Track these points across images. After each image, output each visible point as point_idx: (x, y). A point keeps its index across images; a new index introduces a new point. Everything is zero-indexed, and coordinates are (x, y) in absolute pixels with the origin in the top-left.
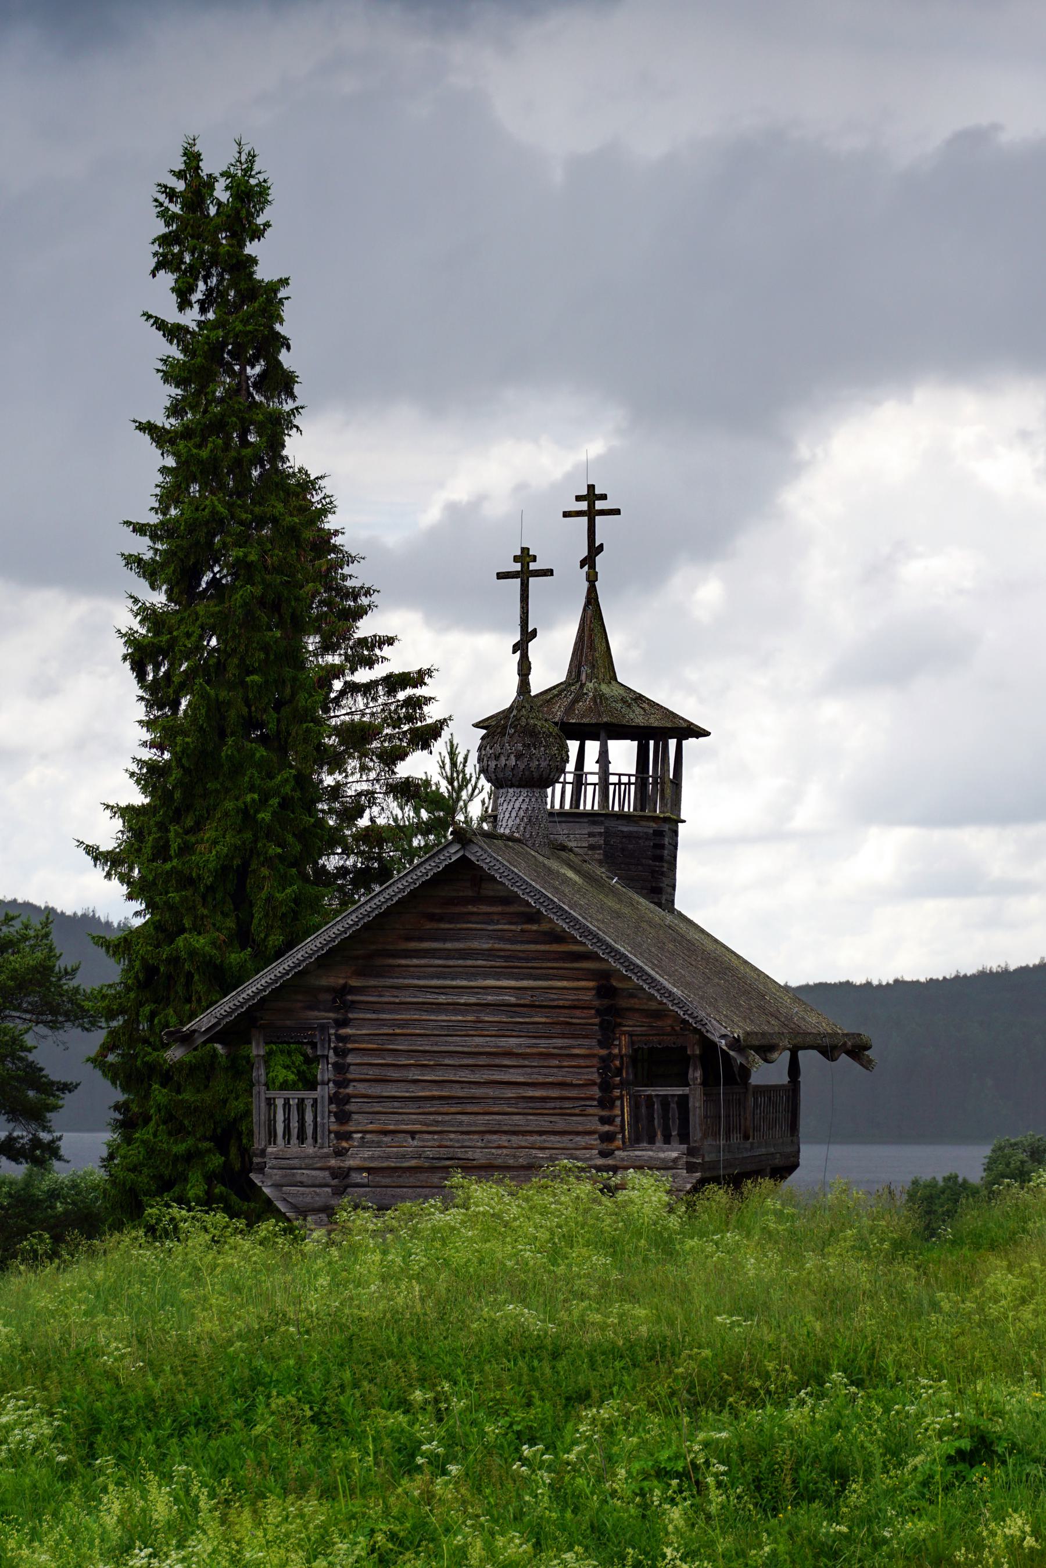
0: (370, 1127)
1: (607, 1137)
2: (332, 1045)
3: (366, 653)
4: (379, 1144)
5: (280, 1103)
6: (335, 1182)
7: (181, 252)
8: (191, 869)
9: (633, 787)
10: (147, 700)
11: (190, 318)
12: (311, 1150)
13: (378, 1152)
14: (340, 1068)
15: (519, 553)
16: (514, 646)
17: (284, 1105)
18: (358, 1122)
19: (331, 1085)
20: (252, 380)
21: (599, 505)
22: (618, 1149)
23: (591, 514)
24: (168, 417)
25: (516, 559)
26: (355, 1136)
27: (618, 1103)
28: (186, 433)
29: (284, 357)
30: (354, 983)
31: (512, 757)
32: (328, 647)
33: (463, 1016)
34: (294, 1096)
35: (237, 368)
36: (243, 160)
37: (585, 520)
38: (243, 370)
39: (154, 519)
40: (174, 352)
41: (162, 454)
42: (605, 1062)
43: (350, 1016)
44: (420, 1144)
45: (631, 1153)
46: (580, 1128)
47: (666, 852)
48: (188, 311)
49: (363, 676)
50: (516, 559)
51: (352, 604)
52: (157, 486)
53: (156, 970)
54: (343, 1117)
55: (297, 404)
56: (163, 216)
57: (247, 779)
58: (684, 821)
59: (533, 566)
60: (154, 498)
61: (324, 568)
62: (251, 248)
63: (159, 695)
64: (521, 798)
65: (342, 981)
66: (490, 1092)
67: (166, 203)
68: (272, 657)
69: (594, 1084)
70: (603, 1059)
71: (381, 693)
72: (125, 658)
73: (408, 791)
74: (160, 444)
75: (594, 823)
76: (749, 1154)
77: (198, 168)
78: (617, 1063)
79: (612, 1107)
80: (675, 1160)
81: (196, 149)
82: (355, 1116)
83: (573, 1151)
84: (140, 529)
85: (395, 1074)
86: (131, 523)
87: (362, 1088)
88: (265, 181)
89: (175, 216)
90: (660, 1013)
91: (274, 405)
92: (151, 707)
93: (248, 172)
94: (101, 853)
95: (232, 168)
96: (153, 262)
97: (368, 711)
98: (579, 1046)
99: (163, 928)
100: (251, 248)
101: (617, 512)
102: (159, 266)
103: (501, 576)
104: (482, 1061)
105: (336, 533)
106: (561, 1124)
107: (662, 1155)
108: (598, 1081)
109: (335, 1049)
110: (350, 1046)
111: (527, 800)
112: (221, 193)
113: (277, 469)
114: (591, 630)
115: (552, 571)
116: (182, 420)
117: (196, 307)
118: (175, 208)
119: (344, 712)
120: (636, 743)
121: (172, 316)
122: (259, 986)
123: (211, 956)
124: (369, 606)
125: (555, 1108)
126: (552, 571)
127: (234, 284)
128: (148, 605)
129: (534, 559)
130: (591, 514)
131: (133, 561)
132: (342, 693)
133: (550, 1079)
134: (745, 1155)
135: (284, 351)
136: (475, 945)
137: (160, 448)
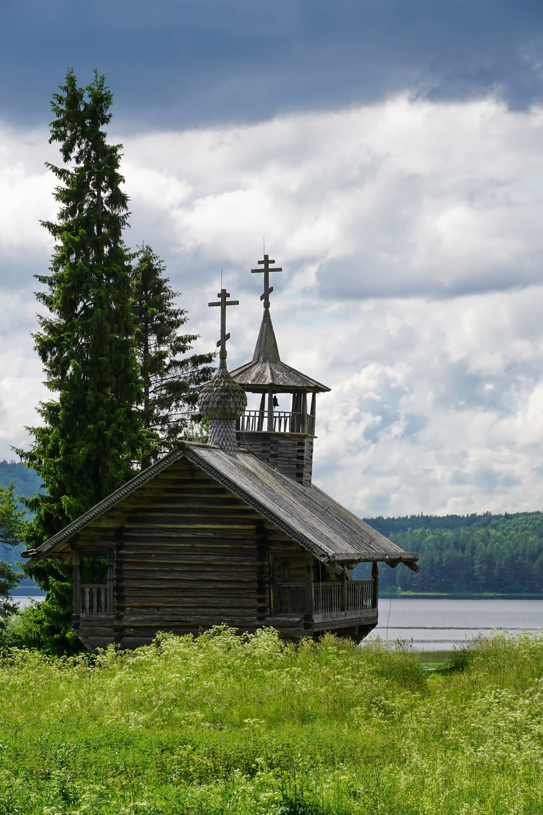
0: (135, 604)
1: (262, 610)
2: (115, 560)
3: (182, 344)
4: (140, 613)
5: (87, 590)
6: (115, 634)
7: (66, 131)
8: (70, 462)
9: (257, 418)
10: (49, 371)
11: (71, 166)
12: (103, 616)
13: (139, 618)
14: (119, 571)
15: (220, 292)
16: (218, 343)
17: (89, 592)
18: (128, 602)
19: (114, 581)
20: (105, 199)
21: (271, 266)
22: (268, 616)
24: (59, 219)
25: (219, 295)
26: (127, 609)
27: (268, 591)
28: (68, 228)
30: (127, 526)
31: (215, 403)
32: (160, 342)
33: (185, 544)
34: (95, 588)
35: (96, 193)
36: (98, 81)
38: (99, 193)
39: (51, 274)
40: (63, 184)
41: (55, 239)
42: (261, 569)
43: (125, 544)
44: (162, 613)
45: (275, 619)
46: (248, 605)
47: (305, 454)
48: (69, 162)
49: (180, 357)
50: (219, 295)
51: (174, 319)
52: (52, 256)
54: (120, 598)
55: (129, 211)
56: (56, 111)
57: (99, 413)
58: (316, 437)
59: (228, 299)
60: (51, 262)
61: (158, 300)
62: (102, 129)
63: (57, 368)
64: (220, 426)
65: (120, 525)
66: (200, 585)
67: (57, 104)
68: (114, 348)
69: (255, 581)
70: (259, 567)
71: (190, 366)
72: (35, 349)
74: (54, 233)
76: (344, 618)
77: (74, 85)
78: (267, 570)
80: (298, 622)
81: (73, 75)
82: (127, 598)
83: (244, 618)
84: (43, 280)
85: (149, 575)
86: (38, 276)
88: (109, 92)
89: (62, 111)
90: (290, 543)
91: (116, 212)
92: (50, 375)
93: (101, 87)
94: (24, 453)
95: (92, 85)
96: (50, 135)
97: (182, 376)
98: (247, 560)
100: (102, 129)
101: (280, 270)
102: (54, 137)
103: (211, 305)
105: (166, 281)
107: (291, 619)
108: (257, 579)
109: (117, 562)
110: (125, 560)
111: (224, 426)
112: (87, 99)
113: (118, 247)
114: (266, 334)
115: (238, 302)
116: (66, 221)
117: (74, 160)
118: (63, 107)
119: (170, 376)
120: (292, 394)
121: (62, 165)
122: (74, 527)
123: (79, 508)
124: (185, 319)
125: (234, 594)
126: (238, 302)
127: (94, 148)
128: (48, 320)
129: (229, 295)
130: (267, 271)
131: (41, 296)
132: (170, 366)
134: (341, 619)
135: (121, 183)
136: (191, 506)
137: (55, 235)
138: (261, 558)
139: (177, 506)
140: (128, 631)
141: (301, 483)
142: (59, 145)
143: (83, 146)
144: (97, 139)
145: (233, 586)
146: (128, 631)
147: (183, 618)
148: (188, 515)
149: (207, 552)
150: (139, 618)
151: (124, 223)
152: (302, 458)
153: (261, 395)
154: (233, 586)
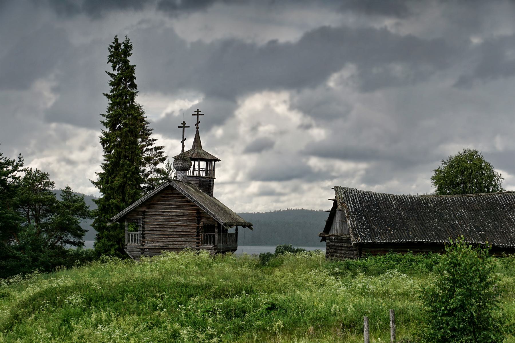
1: (198, 243)
11: (115, 72)
13: (151, 245)
14: (143, 228)
18: (147, 239)
21: (199, 113)
23: (198, 115)
28: (114, 96)
29: (135, 81)
34: (134, 233)
37: (196, 116)
39: (107, 114)
42: (198, 227)
49: (150, 147)
53: (106, 207)
54: (144, 238)
62: (128, 58)
63: (107, 150)
66: (174, 233)
73: (158, 171)
84: (104, 116)
85: (154, 229)
87: (148, 232)
89: (112, 51)
90: (209, 218)
91: (132, 91)
93: (128, 42)
99: (107, 198)
100: (128, 58)
101: (203, 115)
103: (179, 127)
104: (173, 227)
106: (188, 240)
112: (122, 47)
118: (113, 50)
121: (112, 72)
130: (198, 115)
136: (172, 203)
138: (198, 223)
140: (146, 250)
142: (111, 64)
143: (120, 65)
144: (126, 62)
145: (187, 234)
146: (146, 250)
149: (177, 221)
150: (151, 245)
151: (136, 95)
152: (210, 186)
154: (187, 234)
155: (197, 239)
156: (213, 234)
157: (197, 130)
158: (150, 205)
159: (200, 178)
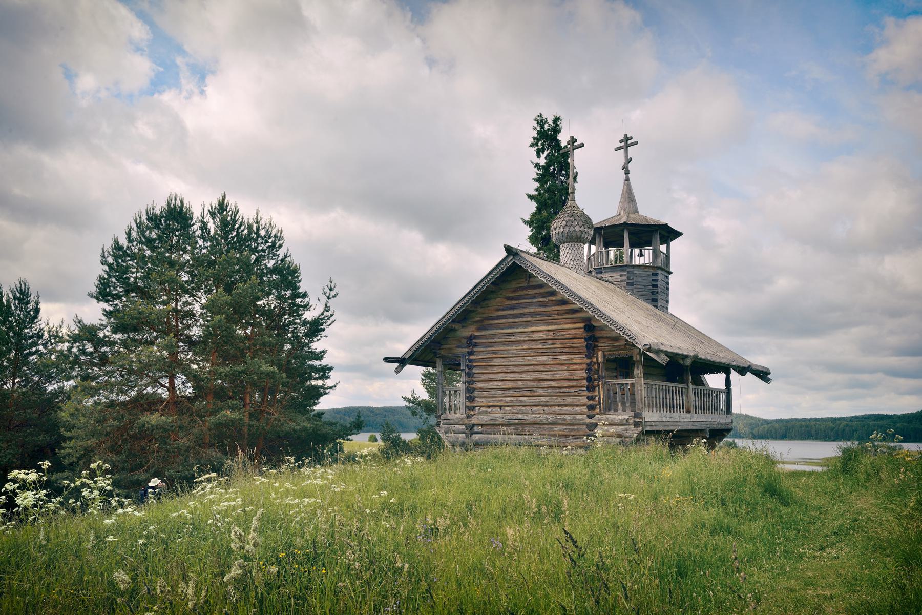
0: (482, 404)
1: (591, 408)
4: (486, 413)
30: (477, 334)
54: (471, 399)
75: (622, 270)
78: (596, 367)
79: (594, 391)
80: (627, 420)
90: (617, 338)
101: (637, 143)
104: (531, 368)
106: (568, 400)
121: (537, 161)
133: (562, 377)
136: (527, 310)
139: (516, 312)
141: (656, 307)
146: (476, 429)
147: (520, 416)
148: (525, 319)
153: (723, 376)
155: (589, 398)
156: (629, 381)
157: (627, 179)
158: (482, 321)
159: (631, 270)
